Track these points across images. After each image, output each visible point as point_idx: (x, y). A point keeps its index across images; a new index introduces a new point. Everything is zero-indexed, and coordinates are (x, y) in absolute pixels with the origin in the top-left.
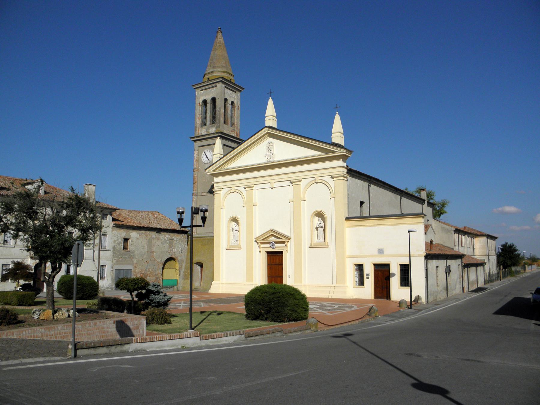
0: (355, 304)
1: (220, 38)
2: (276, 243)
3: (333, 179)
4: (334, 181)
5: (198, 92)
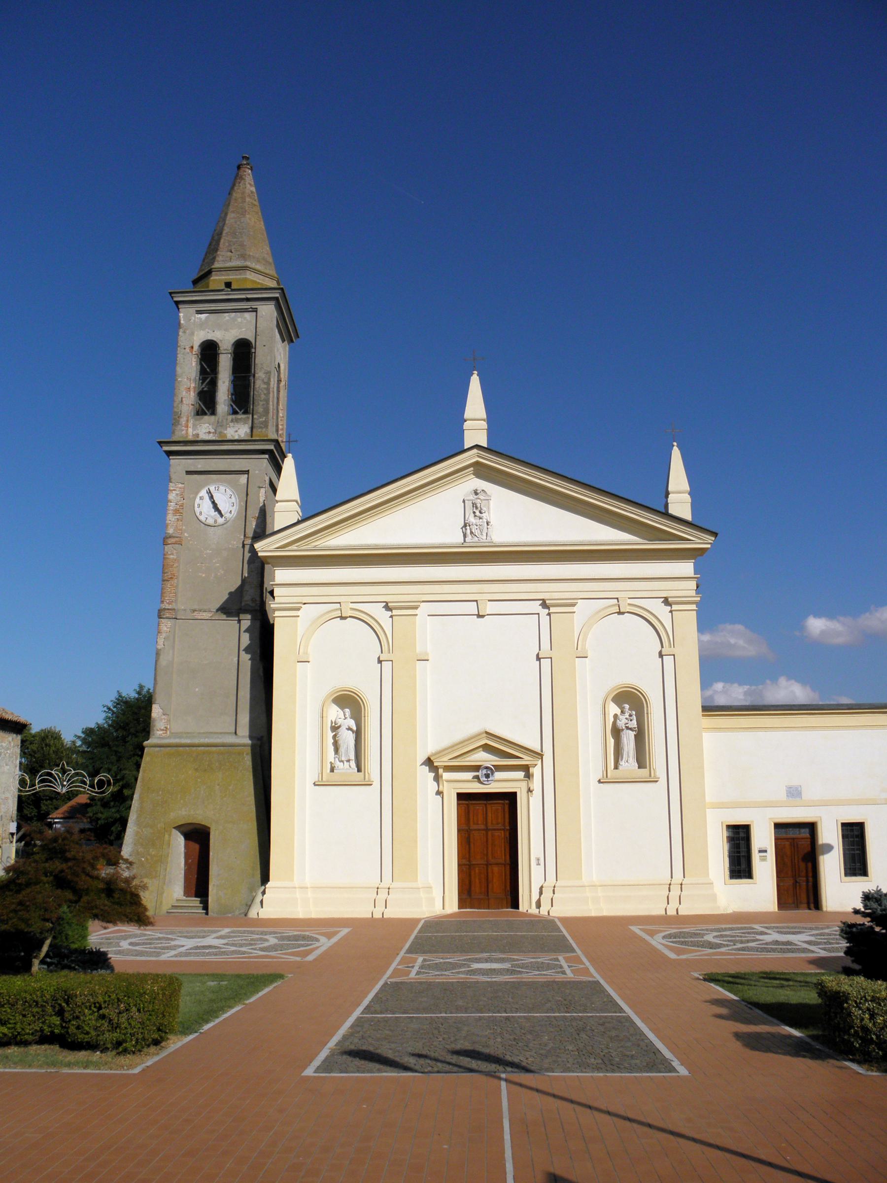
0: (271, 933)
1: (248, 184)
2: (499, 768)
3: (389, 613)
4: (391, 617)
5: (186, 315)
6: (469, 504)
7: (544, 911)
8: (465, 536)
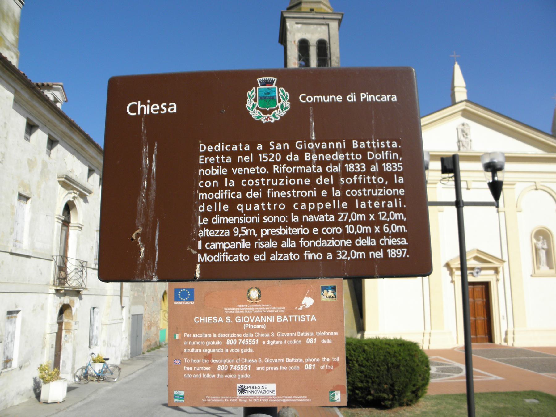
6: (460, 131)
7: (510, 343)
8: (459, 147)
